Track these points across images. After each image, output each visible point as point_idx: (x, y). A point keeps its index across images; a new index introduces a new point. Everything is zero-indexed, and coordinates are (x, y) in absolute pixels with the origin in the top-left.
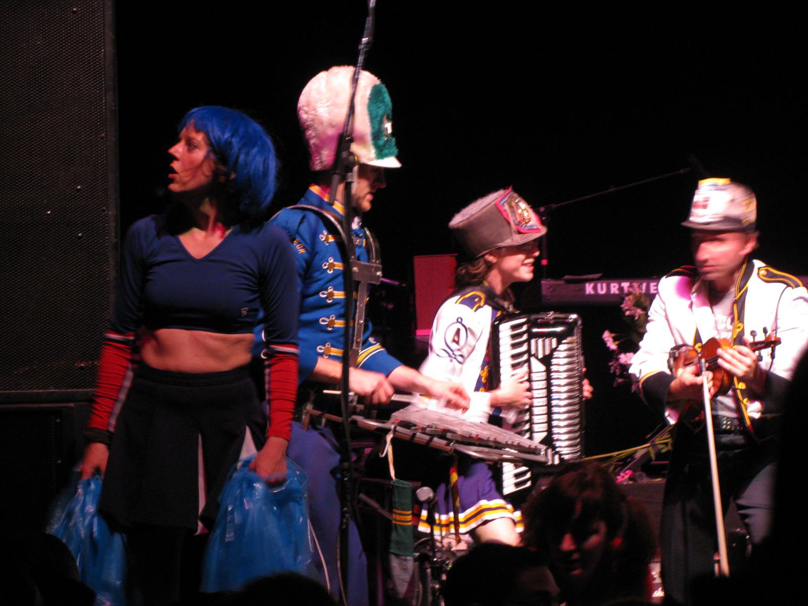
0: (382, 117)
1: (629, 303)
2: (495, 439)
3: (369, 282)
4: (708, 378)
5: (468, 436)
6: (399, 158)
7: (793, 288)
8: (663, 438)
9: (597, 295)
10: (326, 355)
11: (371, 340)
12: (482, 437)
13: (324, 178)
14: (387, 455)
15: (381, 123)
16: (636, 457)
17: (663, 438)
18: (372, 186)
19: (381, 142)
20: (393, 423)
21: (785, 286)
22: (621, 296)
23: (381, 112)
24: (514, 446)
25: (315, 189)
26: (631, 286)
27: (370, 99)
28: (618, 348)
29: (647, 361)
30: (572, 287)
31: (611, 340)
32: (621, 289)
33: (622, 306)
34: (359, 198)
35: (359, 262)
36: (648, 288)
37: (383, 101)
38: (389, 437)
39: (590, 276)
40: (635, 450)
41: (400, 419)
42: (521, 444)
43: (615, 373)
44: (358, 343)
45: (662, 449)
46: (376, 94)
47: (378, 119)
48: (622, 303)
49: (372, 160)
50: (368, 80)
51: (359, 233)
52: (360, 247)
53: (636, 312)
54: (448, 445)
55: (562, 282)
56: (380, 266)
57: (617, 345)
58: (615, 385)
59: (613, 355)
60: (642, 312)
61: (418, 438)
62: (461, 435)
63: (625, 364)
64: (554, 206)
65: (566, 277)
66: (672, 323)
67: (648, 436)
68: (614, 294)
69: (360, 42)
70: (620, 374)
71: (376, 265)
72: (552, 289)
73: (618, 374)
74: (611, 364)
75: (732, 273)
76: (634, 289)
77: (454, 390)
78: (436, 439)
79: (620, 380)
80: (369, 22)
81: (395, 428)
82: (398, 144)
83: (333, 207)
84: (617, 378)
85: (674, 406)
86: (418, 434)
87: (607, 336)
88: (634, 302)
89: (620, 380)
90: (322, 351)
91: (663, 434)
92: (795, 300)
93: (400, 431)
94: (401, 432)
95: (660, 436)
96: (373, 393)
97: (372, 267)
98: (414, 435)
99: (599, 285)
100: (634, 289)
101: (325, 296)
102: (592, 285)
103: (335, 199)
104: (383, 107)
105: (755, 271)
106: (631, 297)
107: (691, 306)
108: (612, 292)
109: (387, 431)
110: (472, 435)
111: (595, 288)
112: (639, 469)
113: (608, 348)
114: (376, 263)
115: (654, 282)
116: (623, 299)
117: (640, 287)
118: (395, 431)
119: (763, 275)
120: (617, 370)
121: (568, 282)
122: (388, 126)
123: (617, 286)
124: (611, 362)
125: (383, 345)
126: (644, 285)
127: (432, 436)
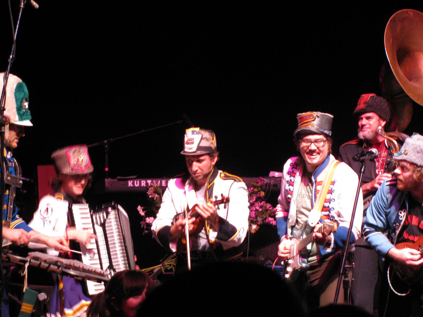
0: (22, 99)
1: (151, 191)
3: (16, 186)
6: (32, 121)
7: (238, 182)
8: (169, 261)
9: (134, 187)
11: (17, 216)
15: (22, 102)
16: (154, 272)
17: (169, 261)
18: (17, 135)
19: (21, 112)
21: (233, 181)
22: (147, 187)
23: (22, 96)
24: (93, 272)
26: (152, 182)
27: (15, 90)
28: (145, 214)
29: (161, 221)
30: (121, 182)
31: (142, 210)
32: (147, 184)
33: (148, 193)
34: (10, 141)
35: (11, 175)
36: (161, 183)
37: (23, 91)
38: (27, 265)
39: (131, 177)
40: (154, 268)
42: (96, 271)
43: (143, 227)
44: (9, 218)
45: (168, 267)
46: (19, 87)
47: (20, 100)
48: (148, 191)
49: (17, 121)
50: (14, 80)
51: (10, 160)
52: (12, 167)
53: (155, 196)
54: (58, 268)
55: (116, 180)
57: (144, 213)
58: (143, 234)
59: (143, 218)
63: (149, 223)
64: (112, 140)
65: (118, 177)
66: (175, 203)
67: (161, 261)
68: (143, 186)
69: (9, 57)
70: (146, 228)
72: (111, 184)
73: (145, 228)
74: (141, 223)
75: (206, 176)
76: (154, 184)
77: (60, 242)
78: (52, 266)
79: (146, 232)
80: (14, 47)
81: (30, 260)
82: (32, 114)
84: (145, 231)
85: (173, 241)
86: (43, 264)
87: (139, 208)
89: (146, 232)
91: (169, 259)
92: (239, 188)
95: (167, 261)
96: (20, 238)
97: (17, 178)
98: (40, 264)
99: (135, 182)
100: (154, 184)
102: (132, 182)
104: (23, 94)
105: (219, 174)
106: (152, 188)
107: (185, 193)
108: (142, 185)
109: (25, 262)
111: (133, 183)
112: (156, 278)
114: (19, 176)
115: (164, 180)
116: (148, 189)
117: (157, 183)
119: (222, 177)
120: (145, 226)
121: (119, 180)
122: (26, 104)
123: (145, 182)
124: (142, 222)
125: (24, 219)
126: (159, 181)
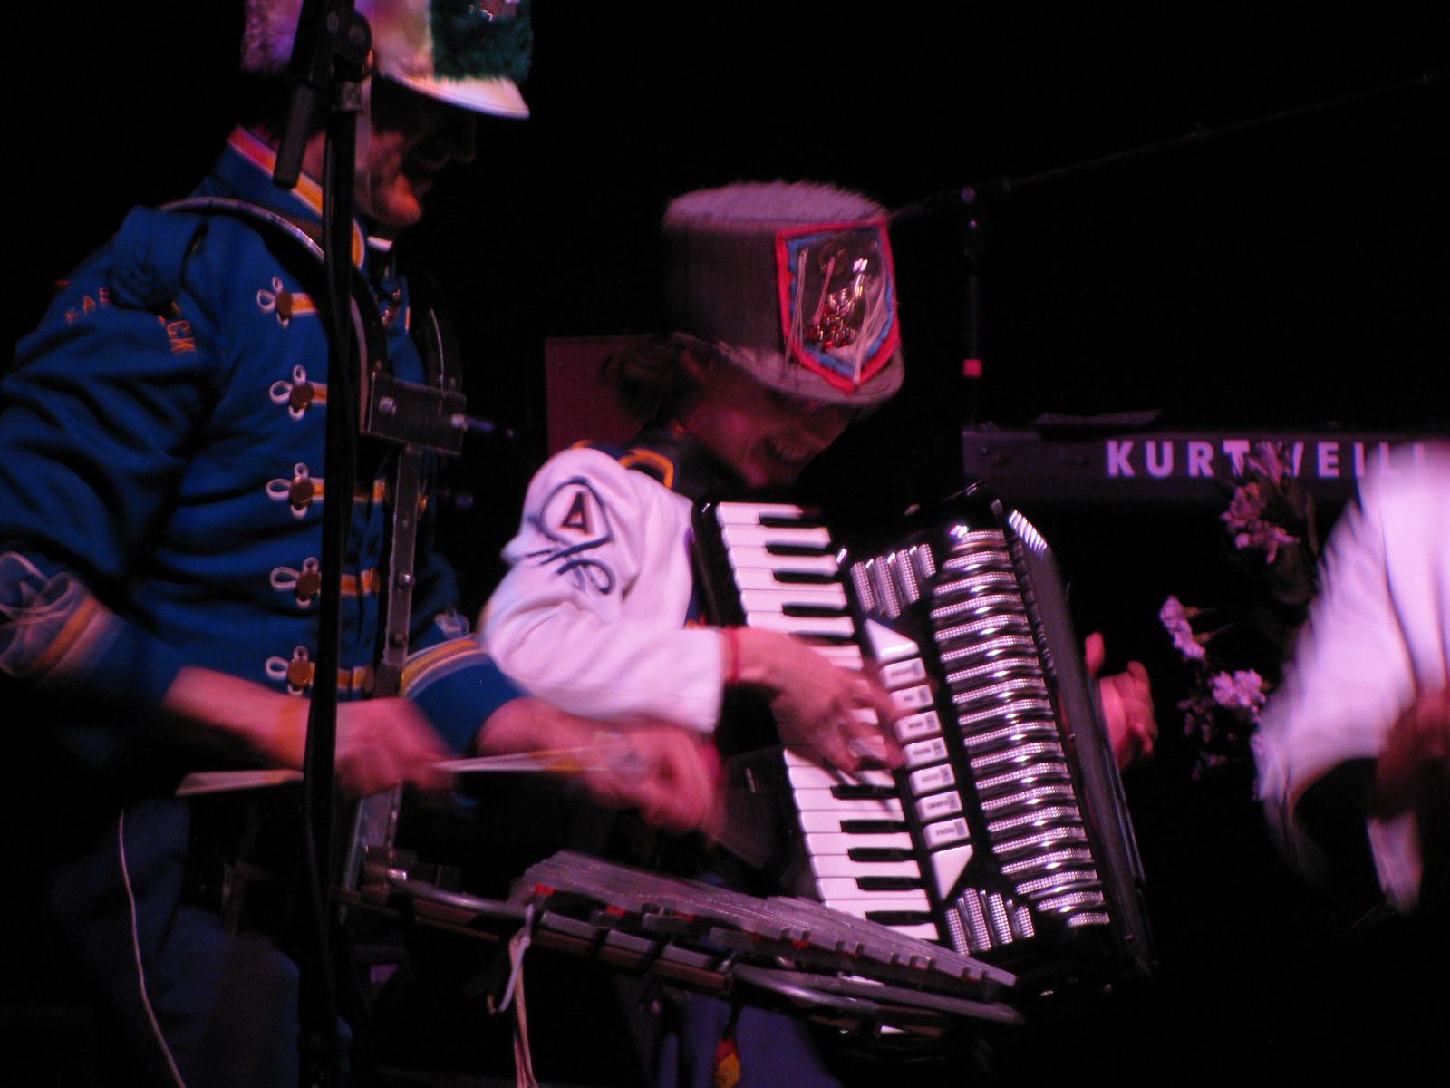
2: (860, 947)
4: (600, 502)
5: (777, 937)
10: (295, 689)
12: (822, 943)
13: (264, 101)
14: (513, 1003)
20: (531, 900)
22: (1224, 482)
25: (250, 148)
26: (1254, 453)
32: (1221, 461)
33: (1226, 516)
38: (518, 948)
39: (1124, 418)
41: (554, 887)
43: (1197, 733)
54: (713, 966)
55: (1031, 436)
56: (459, 396)
60: (1288, 539)
61: (614, 946)
62: (754, 935)
65: (1045, 419)
71: (445, 394)
74: (1183, 705)
78: (671, 950)
79: (1213, 760)
81: (538, 915)
83: (295, 192)
88: (1263, 505)
89: (1213, 760)
90: (282, 675)
93: (551, 924)
94: (561, 928)
98: (602, 935)
99: (1151, 448)
101: (284, 495)
102: (1127, 446)
103: (298, 169)
106: (1254, 489)
108: (1193, 471)
109: (511, 926)
110: (791, 935)
111: (1137, 458)
113: (1180, 652)
116: (1230, 495)
117: (1283, 458)
118: (537, 925)
120: (1205, 728)
121: (1049, 434)
124: (1186, 698)
126: (1298, 449)
127: (660, 939)
